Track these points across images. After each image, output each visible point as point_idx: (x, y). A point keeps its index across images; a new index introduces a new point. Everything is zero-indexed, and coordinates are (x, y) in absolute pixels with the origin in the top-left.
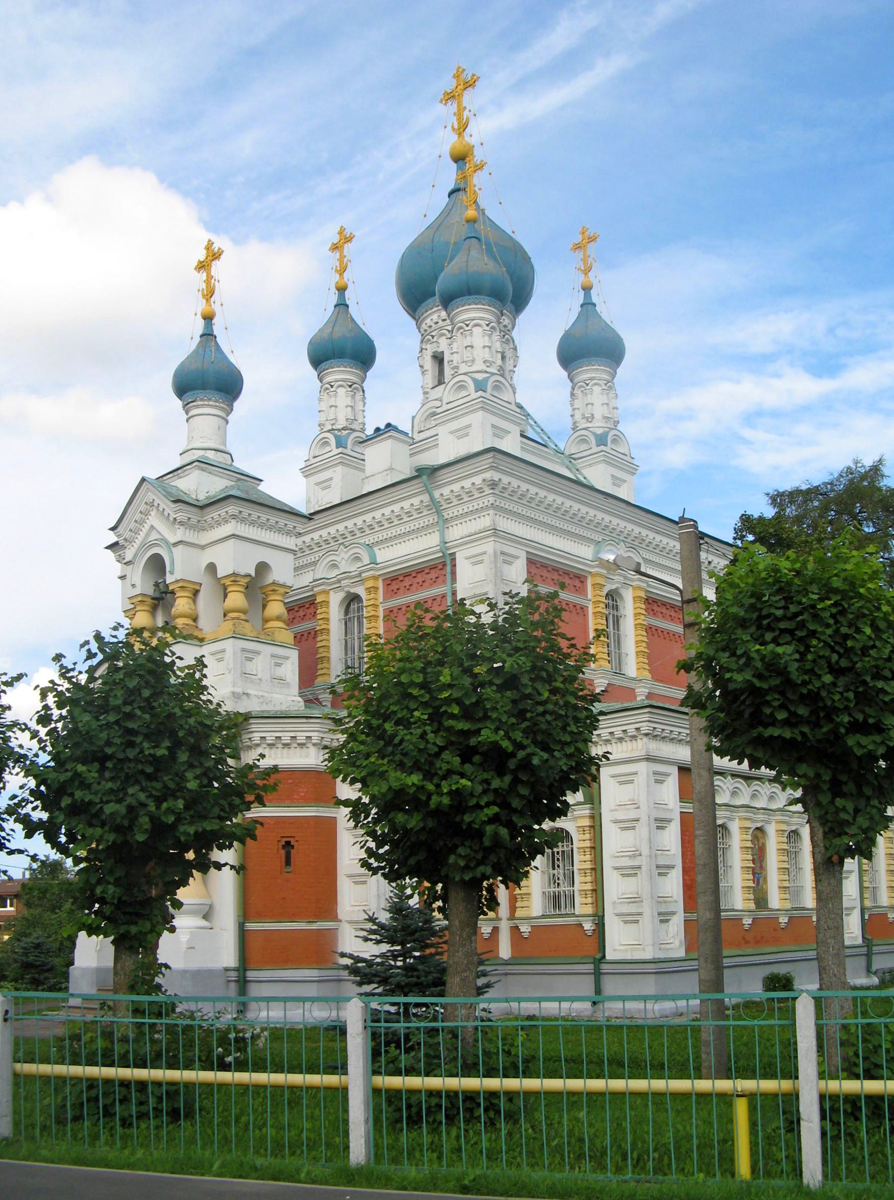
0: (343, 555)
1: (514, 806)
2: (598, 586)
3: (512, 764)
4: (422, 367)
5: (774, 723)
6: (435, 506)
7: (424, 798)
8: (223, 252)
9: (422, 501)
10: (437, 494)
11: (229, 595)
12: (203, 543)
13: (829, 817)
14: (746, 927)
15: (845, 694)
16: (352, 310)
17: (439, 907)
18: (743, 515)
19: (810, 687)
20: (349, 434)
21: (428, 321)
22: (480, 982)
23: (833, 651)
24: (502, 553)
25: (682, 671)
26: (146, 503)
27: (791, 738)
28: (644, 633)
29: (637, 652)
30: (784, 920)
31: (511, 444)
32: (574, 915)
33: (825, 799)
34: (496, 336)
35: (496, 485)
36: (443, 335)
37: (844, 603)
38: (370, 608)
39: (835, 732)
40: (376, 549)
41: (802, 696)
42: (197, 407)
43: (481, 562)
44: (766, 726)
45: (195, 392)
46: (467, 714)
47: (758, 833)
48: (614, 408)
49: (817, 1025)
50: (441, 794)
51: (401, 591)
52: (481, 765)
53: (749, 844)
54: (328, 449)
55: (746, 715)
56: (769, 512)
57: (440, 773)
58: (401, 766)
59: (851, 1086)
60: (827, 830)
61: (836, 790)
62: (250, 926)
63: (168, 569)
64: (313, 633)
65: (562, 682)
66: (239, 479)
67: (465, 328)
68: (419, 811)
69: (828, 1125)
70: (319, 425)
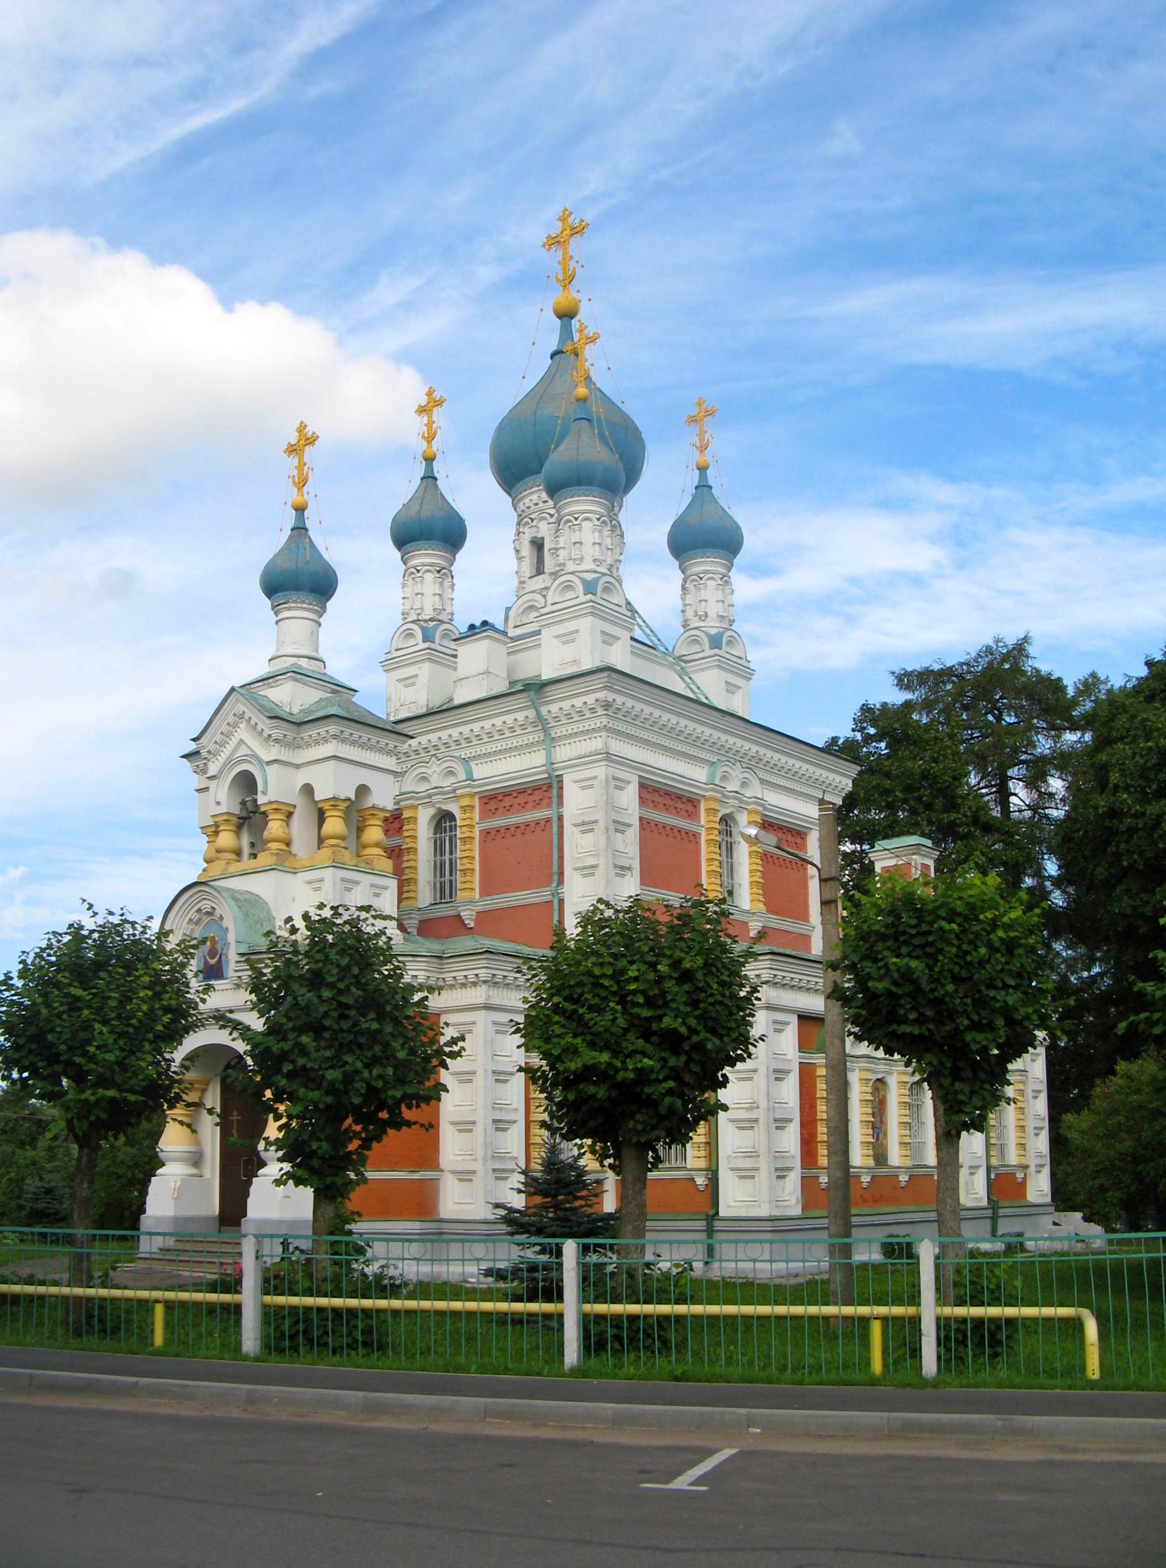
0: (435, 768)
1: (686, 1080)
2: (711, 811)
3: (687, 1046)
4: (517, 551)
5: (905, 1021)
6: (541, 722)
7: (612, 1073)
8: (318, 437)
9: (527, 717)
10: (544, 710)
11: (328, 820)
12: (299, 761)
13: (949, 1097)
14: (865, 1185)
15: (965, 1000)
17: (610, 1164)
18: (864, 705)
19: (936, 994)
20: (437, 627)
21: (527, 501)
23: (956, 963)
24: (615, 778)
25: (830, 970)
26: (235, 715)
27: (920, 1034)
28: (760, 862)
29: (751, 882)
30: (904, 1178)
31: (620, 657)
33: (946, 1082)
34: (606, 532)
35: (610, 706)
36: (544, 518)
37: (965, 924)
38: (464, 829)
39: (956, 1029)
40: (472, 764)
41: (930, 1001)
42: (289, 609)
43: (591, 787)
44: (900, 1023)
45: (287, 593)
46: (650, 1003)
47: (879, 1085)
48: (729, 605)
49: (935, 1263)
50: (626, 1069)
51: (498, 812)
52: (658, 1045)
53: (869, 1097)
54: (412, 642)
55: (884, 1013)
56: (898, 697)
57: (626, 1052)
58: (592, 1045)
59: (960, 1311)
60: (947, 1107)
61: (956, 1075)
63: (260, 788)
64: (397, 850)
65: (729, 976)
66: (338, 692)
67: (574, 521)
68: (604, 1083)
69: (943, 1350)
70: (403, 614)
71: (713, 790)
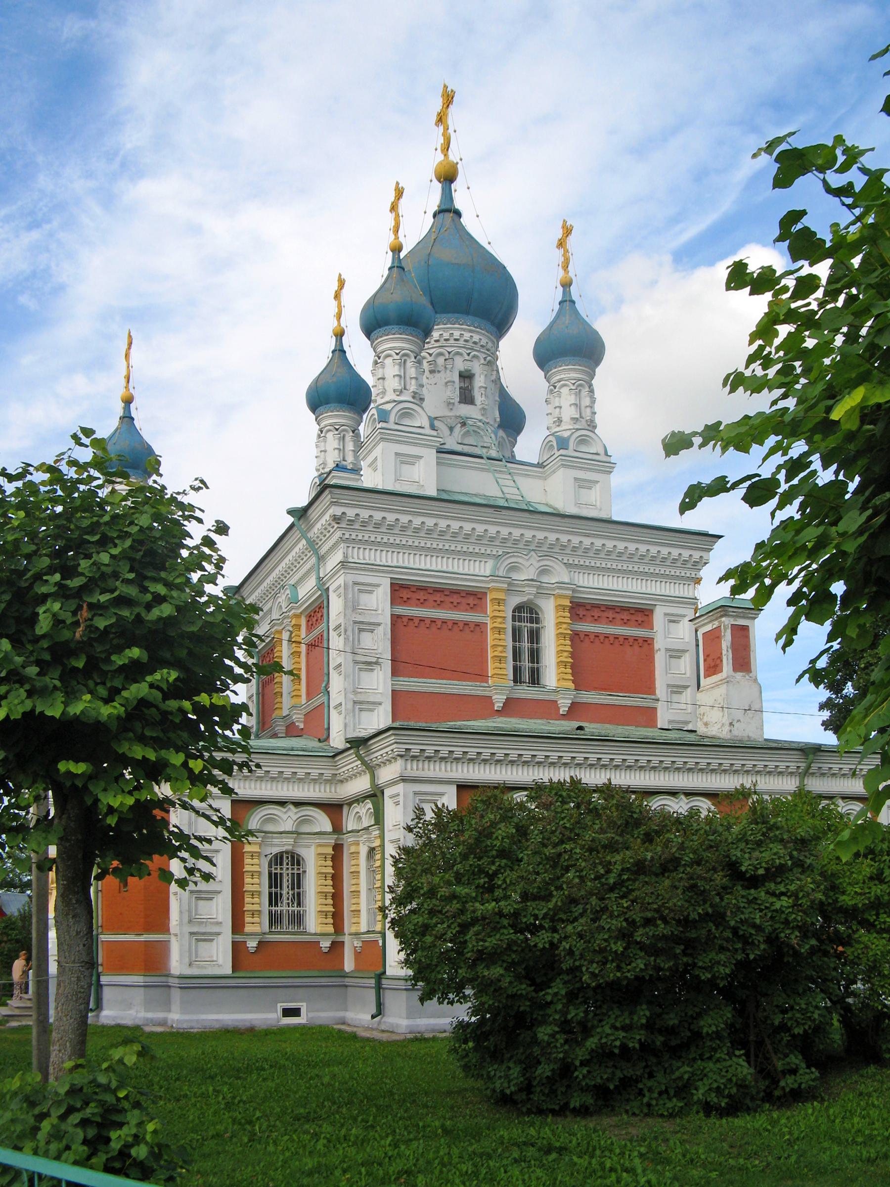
16: (348, 355)
24: (355, 583)
71: (493, 581)
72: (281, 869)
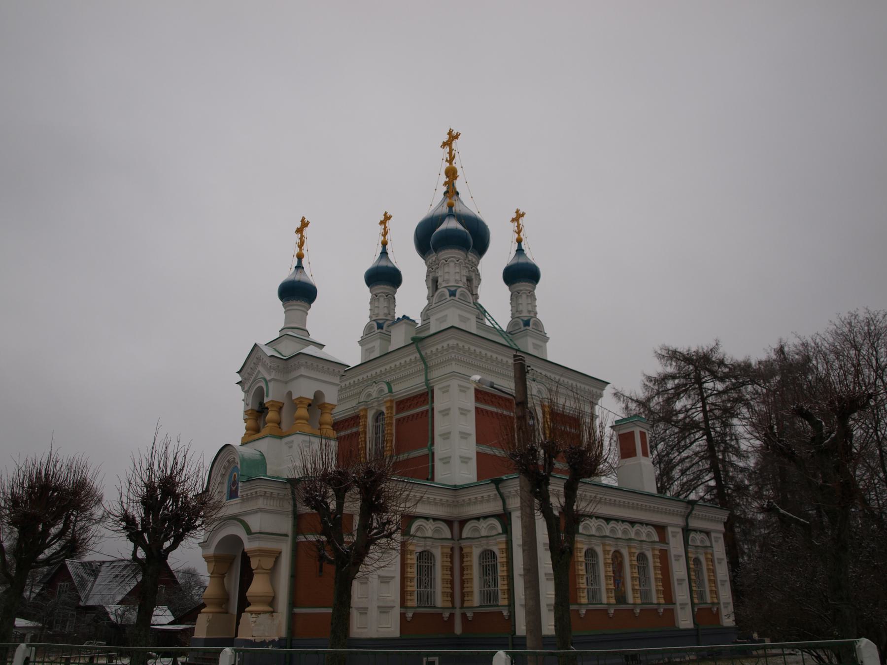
10: (423, 353)
20: (384, 322)
22: (71, 627)
32: (497, 606)
62: (297, 610)
72: (431, 563)
